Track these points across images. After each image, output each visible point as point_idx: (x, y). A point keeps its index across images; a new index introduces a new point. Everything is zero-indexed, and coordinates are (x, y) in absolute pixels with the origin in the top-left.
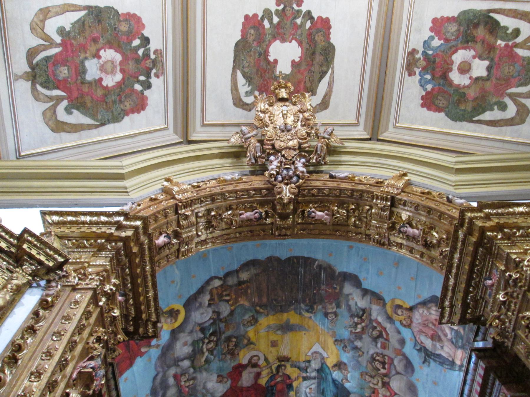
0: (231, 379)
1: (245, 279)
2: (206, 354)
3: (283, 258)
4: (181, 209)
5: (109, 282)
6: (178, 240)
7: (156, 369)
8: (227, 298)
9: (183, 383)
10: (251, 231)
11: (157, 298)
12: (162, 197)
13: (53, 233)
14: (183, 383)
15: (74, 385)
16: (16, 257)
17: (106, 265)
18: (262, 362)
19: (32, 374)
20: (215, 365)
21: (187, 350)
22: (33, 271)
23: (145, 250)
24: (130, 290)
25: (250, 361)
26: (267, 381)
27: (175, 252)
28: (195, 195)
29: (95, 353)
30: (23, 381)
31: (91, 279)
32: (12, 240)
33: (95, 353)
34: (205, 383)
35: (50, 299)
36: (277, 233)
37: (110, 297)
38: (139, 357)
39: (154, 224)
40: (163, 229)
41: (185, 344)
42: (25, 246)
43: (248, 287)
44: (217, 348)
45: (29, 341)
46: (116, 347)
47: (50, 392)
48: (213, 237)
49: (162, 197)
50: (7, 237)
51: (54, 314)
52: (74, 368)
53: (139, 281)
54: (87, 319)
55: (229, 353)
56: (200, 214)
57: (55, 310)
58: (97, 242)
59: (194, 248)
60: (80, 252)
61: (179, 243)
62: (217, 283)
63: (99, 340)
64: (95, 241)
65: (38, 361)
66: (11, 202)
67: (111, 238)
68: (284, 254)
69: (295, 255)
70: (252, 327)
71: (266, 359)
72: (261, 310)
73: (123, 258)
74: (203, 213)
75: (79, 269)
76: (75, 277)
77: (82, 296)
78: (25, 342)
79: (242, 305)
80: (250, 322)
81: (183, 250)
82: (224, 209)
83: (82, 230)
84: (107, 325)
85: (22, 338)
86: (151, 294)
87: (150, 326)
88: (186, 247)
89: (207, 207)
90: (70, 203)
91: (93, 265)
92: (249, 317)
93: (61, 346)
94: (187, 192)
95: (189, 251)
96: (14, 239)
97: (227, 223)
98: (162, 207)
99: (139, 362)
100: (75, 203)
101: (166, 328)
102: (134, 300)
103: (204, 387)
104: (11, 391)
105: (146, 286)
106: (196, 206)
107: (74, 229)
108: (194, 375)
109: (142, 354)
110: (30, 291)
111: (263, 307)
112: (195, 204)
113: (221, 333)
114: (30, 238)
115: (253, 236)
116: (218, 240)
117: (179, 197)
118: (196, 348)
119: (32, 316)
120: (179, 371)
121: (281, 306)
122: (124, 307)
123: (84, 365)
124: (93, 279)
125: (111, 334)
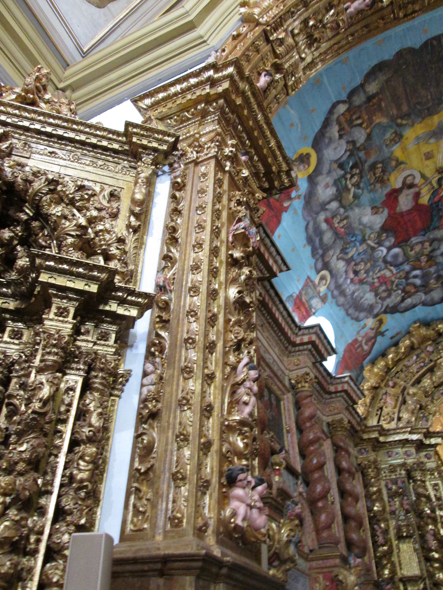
0: (388, 207)
1: (374, 92)
2: (353, 190)
3: (417, 46)
4: (272, 34)
5: (227, 146)
6: (281, 73)
7: (304, 218)
8: (359, 122)
9: (336, 225)
10: (366, 26)
11: (281, 145)
12: (245, 29)
13: (152, 117)
14: (336, 225)
15: (234, 247)
16: (132, 153)
17: (216, 129)
18: (418, 180)
19: (194, 246)
20: (366, 197)
21: (331, 191)
22: (153, 160)
23: (249, 98)
24: (250, 147)
25: (404, 183)
26: (430, 199)
27: (282, 90)
28: (282, 8)
29: (240, 215)
30: (190, 254)
31: (208, 148)
32: (120, 138)
33: (240, 215)
34: (360, 219)
35: (179, 180)
36: (401, 15)
37: (233, 159)
38: (284, 213)
39: (248, 66)
40: (260, 67)
41: (327, 186)
42: (134, 140)
43: (381, 100)
44: (363, 180)
45: (179, 221)
46: (258, 206)
47: (216, 257)
48: (321, 54)
49: (245, 29)
50: (115, 137)
51: (189, 192)
52: (228, 233)
53: (256, 133)
54: (220, 187)
55: (377, 181)
56: (296, 31)
57: (188, 187)
58: (197, 109)
59: (303, 76)
60: (186, 126)
61: (284, 77)
62: (342, 108)
63: (239, 203)
64: (196, 109)
65: (194, 235)
66: (101, 105)
67: (209, 99)
68: (415, 41)
69: (433, 36)
70: (398, 145)
71: (423, 176)
72: (404, 122)
73: (230, 115)
74: (299, 27)
75: (193, 143)
76: (192, 152)
77: (206, 167)
78: (176, 223)
79: (379, 124)
80: (393, 140)
81: (290, 83)
82: (324, 11)
83: (178, 102)
84: (241, 187)
85: (172, 220)
86: (273, 143)
87: (284, 177)
88: (293, 79)
89: (302, 18)
90: (153, 81)
91: (204, 134)
92: (391, 134)
93: (208, 217)
94: (271, 9)
95: (298, 81)
96: (122, 137)
97: (332, 29)
98: (250, 41)
99: (286, 217)
100: (158, 78)
101: (301, 175)
102: (258, 156)
103: (360, 223)
104: (184, 265)
105: (265, 137)
106: (288, 23)
107: (170, 105)
108: (346, 214)
109: (286, 209)
110: (158, 180)
111: (406, 117)
112: (285, 21)
113: (363, 163)
114: (135, 130)
115: (369, 31)
116: (328, 55)
117: (264, 19)
118: (340, 187)
119: (171, 200)
120: (329, 214)
121: (428, 109)
122: (251, 164)
123: (235, 228)
124: (210, 147)
125: (248, 195)
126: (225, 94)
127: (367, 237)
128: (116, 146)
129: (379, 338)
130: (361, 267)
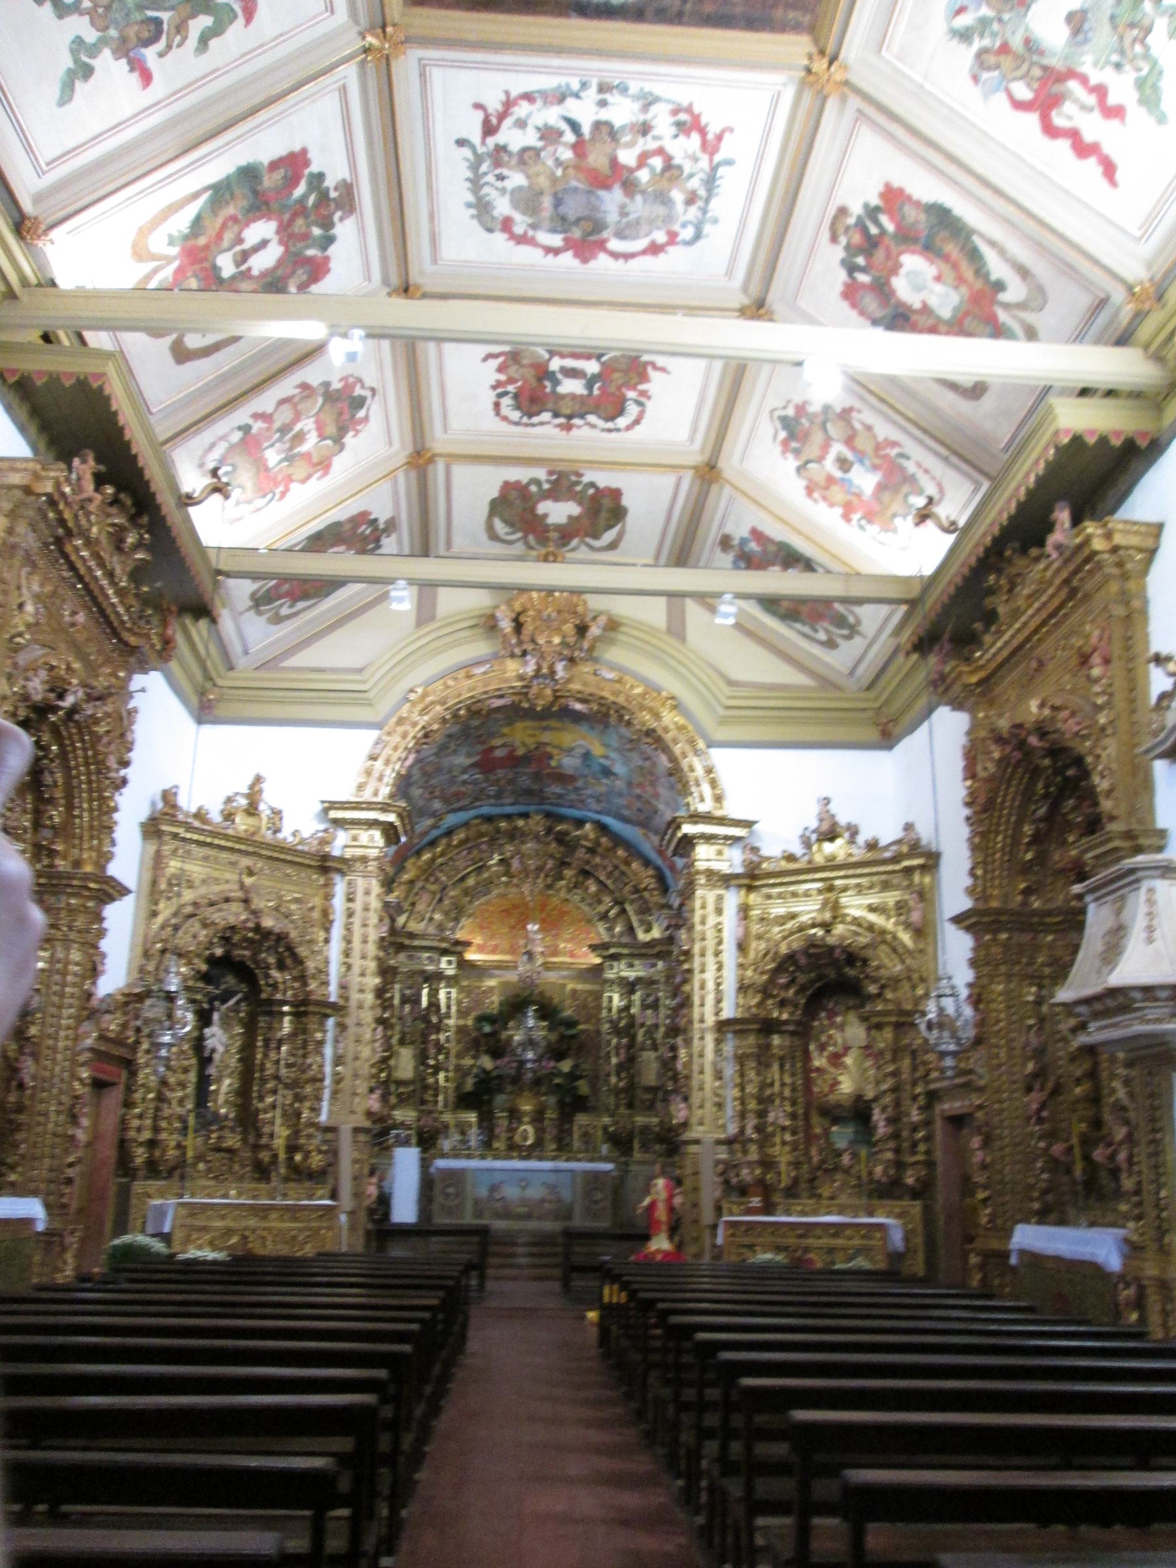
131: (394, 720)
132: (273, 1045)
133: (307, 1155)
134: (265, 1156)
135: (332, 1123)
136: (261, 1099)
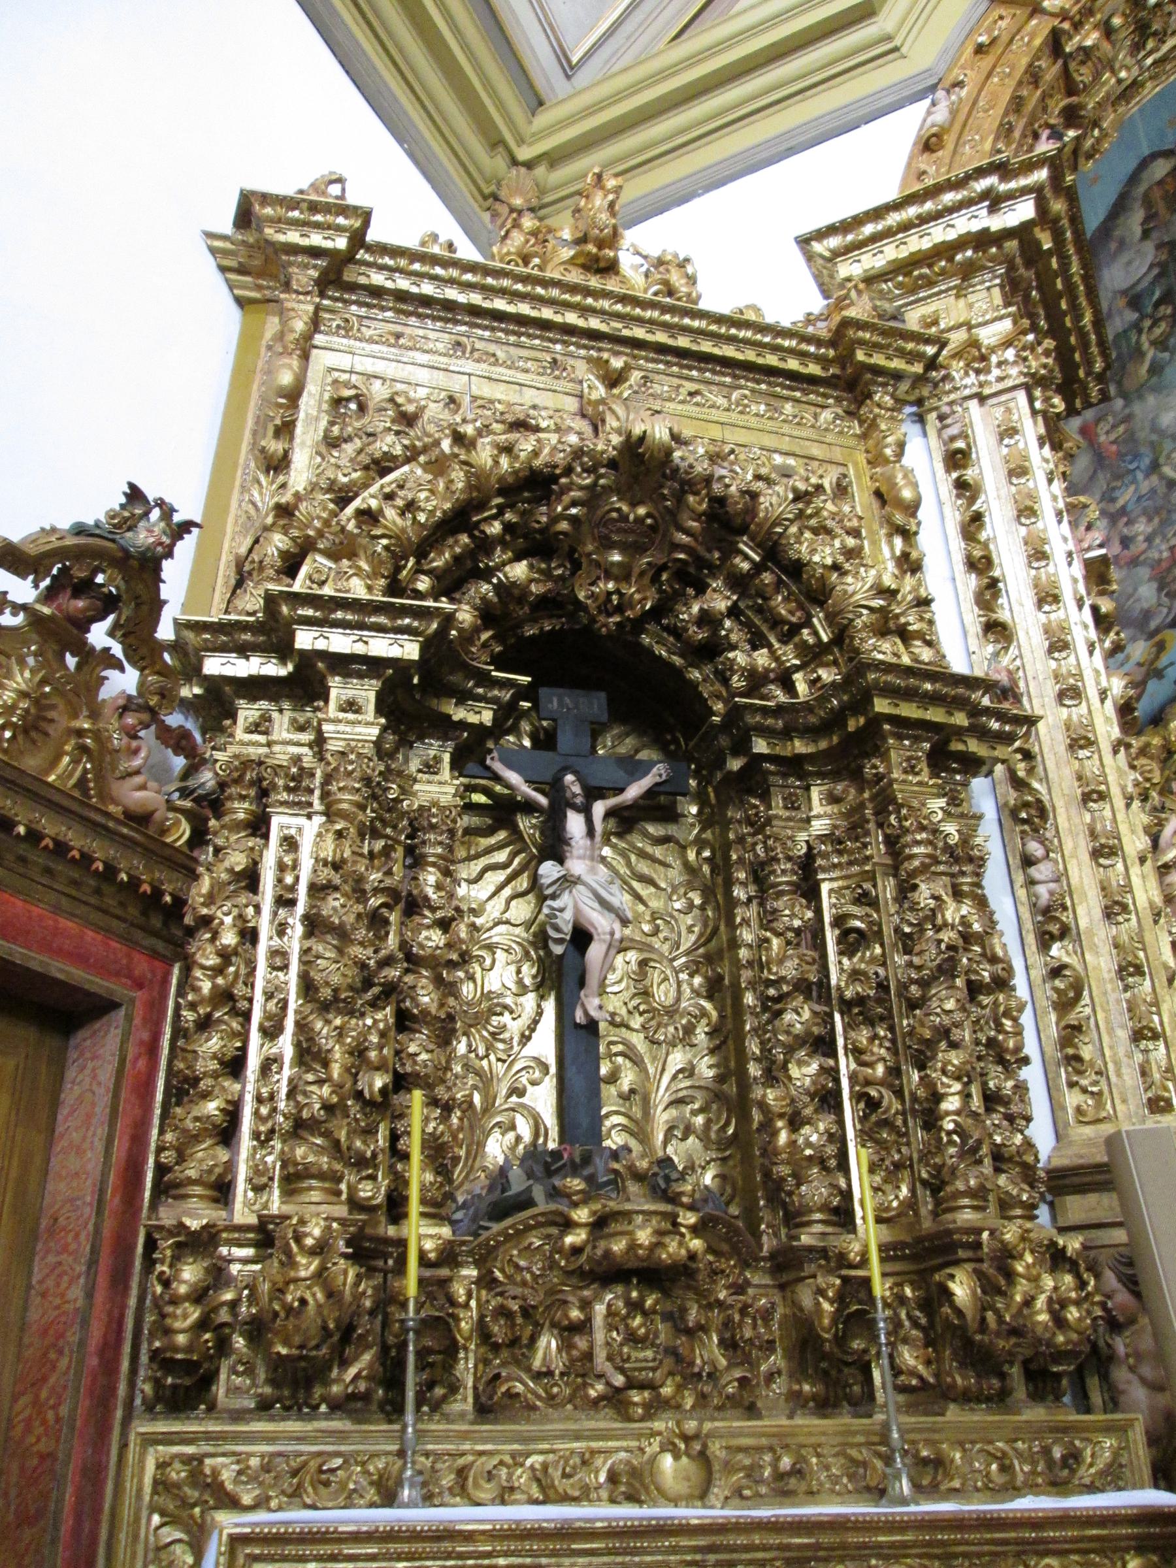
2: (1150, 354)
4: (1070, 38)
9: (1102, 438)
42: (860, 356)
86: (1087, 319)
103: (1155, 428)
126: (1022, 231)
127: (1162, 460)
128: (814, 369)
129: (1152, 685)
130: (1142, 527)
131: (970, 49)
132: (784, 875)
133: (997, 1273)
134: (819, 1299)
135: (1087, 1143)
136: (774, 1074)
